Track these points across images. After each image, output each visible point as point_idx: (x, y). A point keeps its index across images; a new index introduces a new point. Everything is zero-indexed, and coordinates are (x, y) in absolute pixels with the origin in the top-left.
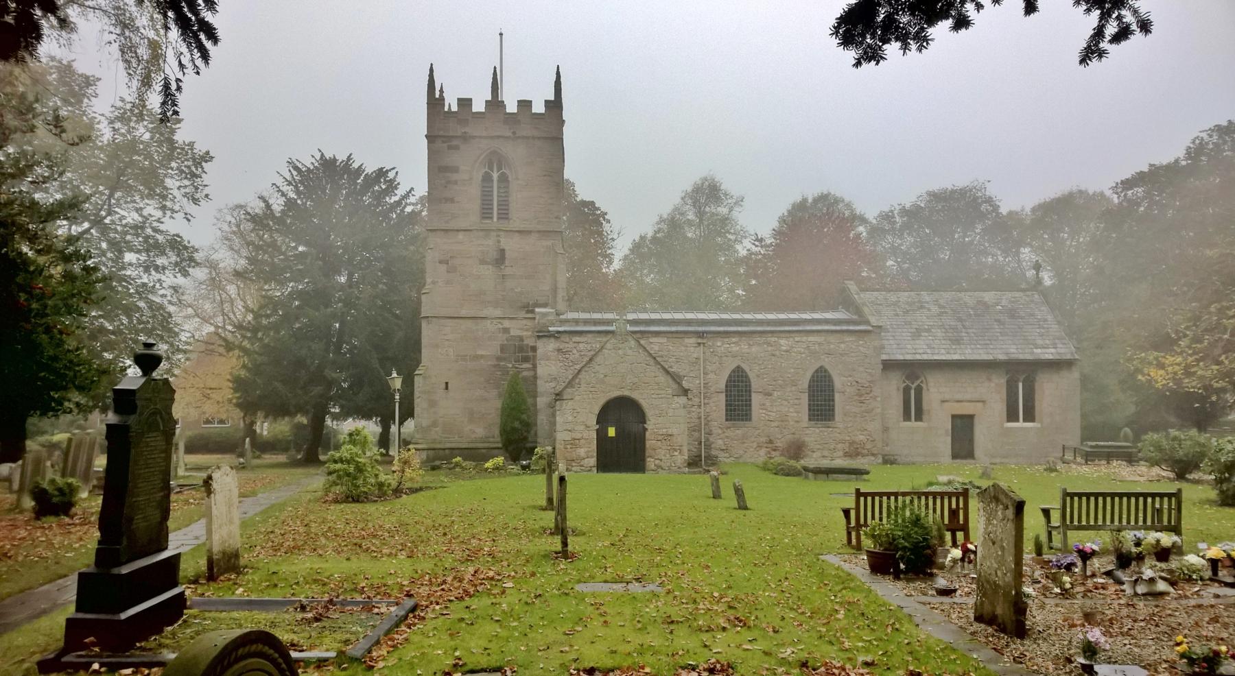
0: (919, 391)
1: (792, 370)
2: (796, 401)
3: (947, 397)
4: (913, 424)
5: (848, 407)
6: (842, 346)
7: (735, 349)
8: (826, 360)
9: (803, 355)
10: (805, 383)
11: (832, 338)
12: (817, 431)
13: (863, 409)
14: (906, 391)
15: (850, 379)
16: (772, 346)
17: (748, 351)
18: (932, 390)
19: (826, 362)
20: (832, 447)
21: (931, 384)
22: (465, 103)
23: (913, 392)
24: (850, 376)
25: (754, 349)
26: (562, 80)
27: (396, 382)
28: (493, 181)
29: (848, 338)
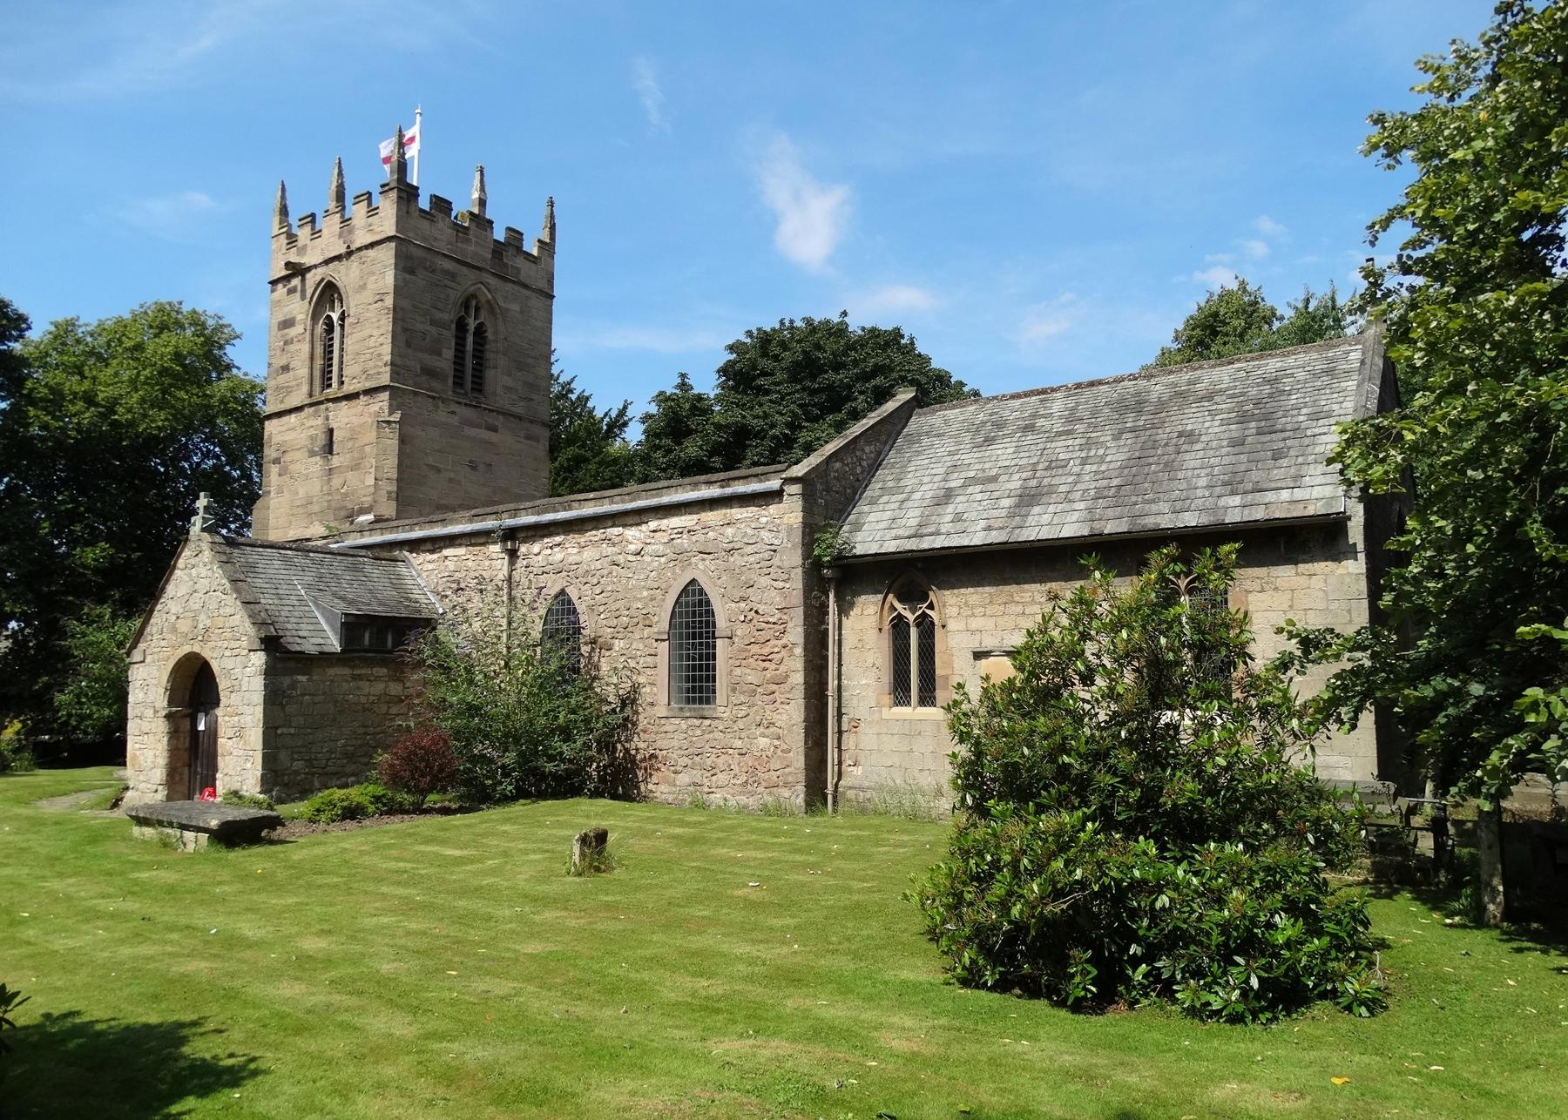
0: (927, 628)
1: (645, 593)
2: (649, 659)
3: (988, 643)
4: (913, 712)
5: (738, 671)
6: (729, 531)
7: (558, 555)
8: (701, 566)
9: (663, 559)
10: (662, 623)
11: (711, 517)
12: (684, 724)
13: (768, 674)
14: (899, 626)
15: (743, 605)
16: (614, 545)
17: (577, 559)
18: (952, 625)
19: (703, 571)
20: (709, 762)
21: (952, 611)
22: (515, 236)
23: (914, 632)
24: (743, 599)
25: (588, 554)
26: (287, 194)
27: (1385, 829)
28: (467, 331)
29: (737, 513)
